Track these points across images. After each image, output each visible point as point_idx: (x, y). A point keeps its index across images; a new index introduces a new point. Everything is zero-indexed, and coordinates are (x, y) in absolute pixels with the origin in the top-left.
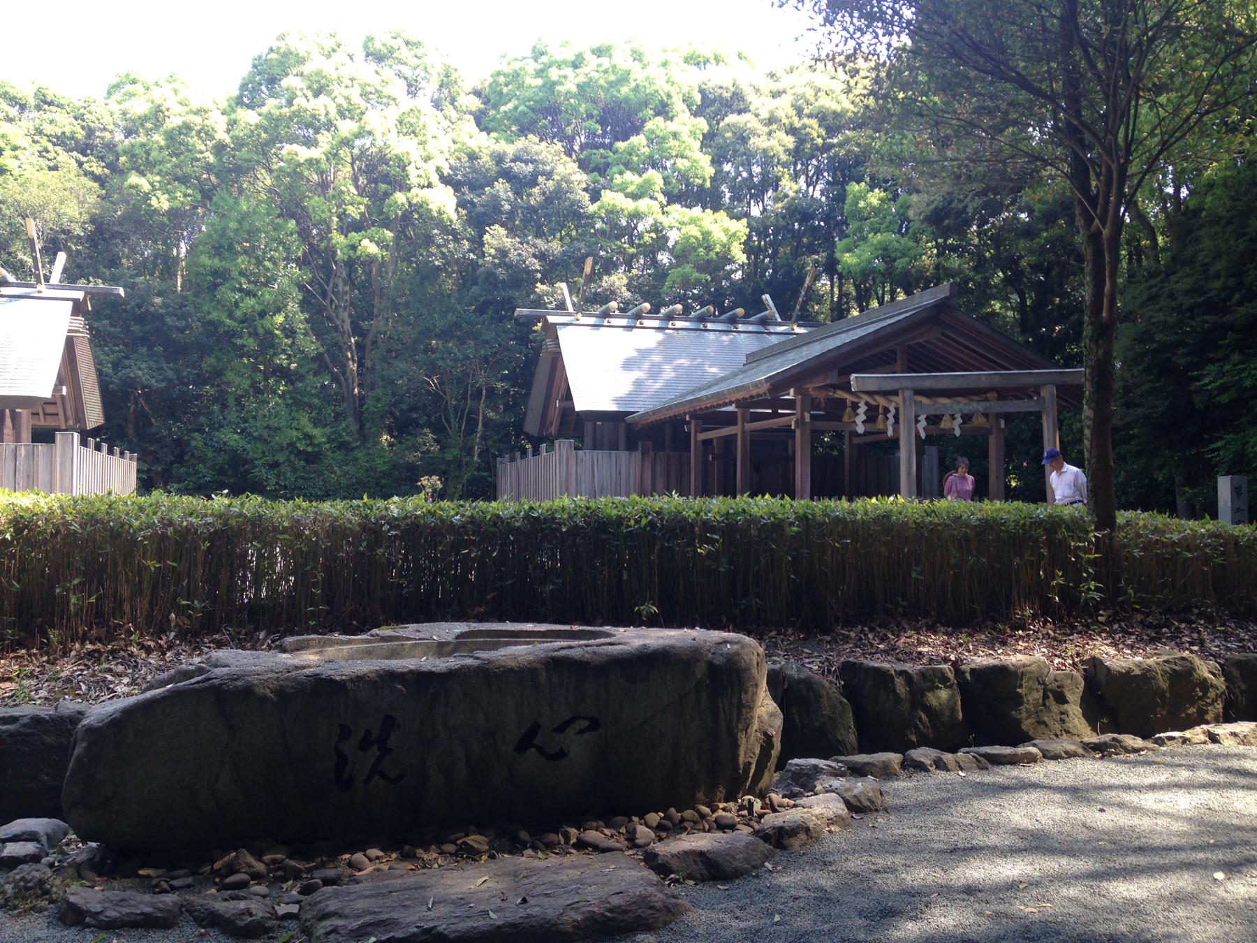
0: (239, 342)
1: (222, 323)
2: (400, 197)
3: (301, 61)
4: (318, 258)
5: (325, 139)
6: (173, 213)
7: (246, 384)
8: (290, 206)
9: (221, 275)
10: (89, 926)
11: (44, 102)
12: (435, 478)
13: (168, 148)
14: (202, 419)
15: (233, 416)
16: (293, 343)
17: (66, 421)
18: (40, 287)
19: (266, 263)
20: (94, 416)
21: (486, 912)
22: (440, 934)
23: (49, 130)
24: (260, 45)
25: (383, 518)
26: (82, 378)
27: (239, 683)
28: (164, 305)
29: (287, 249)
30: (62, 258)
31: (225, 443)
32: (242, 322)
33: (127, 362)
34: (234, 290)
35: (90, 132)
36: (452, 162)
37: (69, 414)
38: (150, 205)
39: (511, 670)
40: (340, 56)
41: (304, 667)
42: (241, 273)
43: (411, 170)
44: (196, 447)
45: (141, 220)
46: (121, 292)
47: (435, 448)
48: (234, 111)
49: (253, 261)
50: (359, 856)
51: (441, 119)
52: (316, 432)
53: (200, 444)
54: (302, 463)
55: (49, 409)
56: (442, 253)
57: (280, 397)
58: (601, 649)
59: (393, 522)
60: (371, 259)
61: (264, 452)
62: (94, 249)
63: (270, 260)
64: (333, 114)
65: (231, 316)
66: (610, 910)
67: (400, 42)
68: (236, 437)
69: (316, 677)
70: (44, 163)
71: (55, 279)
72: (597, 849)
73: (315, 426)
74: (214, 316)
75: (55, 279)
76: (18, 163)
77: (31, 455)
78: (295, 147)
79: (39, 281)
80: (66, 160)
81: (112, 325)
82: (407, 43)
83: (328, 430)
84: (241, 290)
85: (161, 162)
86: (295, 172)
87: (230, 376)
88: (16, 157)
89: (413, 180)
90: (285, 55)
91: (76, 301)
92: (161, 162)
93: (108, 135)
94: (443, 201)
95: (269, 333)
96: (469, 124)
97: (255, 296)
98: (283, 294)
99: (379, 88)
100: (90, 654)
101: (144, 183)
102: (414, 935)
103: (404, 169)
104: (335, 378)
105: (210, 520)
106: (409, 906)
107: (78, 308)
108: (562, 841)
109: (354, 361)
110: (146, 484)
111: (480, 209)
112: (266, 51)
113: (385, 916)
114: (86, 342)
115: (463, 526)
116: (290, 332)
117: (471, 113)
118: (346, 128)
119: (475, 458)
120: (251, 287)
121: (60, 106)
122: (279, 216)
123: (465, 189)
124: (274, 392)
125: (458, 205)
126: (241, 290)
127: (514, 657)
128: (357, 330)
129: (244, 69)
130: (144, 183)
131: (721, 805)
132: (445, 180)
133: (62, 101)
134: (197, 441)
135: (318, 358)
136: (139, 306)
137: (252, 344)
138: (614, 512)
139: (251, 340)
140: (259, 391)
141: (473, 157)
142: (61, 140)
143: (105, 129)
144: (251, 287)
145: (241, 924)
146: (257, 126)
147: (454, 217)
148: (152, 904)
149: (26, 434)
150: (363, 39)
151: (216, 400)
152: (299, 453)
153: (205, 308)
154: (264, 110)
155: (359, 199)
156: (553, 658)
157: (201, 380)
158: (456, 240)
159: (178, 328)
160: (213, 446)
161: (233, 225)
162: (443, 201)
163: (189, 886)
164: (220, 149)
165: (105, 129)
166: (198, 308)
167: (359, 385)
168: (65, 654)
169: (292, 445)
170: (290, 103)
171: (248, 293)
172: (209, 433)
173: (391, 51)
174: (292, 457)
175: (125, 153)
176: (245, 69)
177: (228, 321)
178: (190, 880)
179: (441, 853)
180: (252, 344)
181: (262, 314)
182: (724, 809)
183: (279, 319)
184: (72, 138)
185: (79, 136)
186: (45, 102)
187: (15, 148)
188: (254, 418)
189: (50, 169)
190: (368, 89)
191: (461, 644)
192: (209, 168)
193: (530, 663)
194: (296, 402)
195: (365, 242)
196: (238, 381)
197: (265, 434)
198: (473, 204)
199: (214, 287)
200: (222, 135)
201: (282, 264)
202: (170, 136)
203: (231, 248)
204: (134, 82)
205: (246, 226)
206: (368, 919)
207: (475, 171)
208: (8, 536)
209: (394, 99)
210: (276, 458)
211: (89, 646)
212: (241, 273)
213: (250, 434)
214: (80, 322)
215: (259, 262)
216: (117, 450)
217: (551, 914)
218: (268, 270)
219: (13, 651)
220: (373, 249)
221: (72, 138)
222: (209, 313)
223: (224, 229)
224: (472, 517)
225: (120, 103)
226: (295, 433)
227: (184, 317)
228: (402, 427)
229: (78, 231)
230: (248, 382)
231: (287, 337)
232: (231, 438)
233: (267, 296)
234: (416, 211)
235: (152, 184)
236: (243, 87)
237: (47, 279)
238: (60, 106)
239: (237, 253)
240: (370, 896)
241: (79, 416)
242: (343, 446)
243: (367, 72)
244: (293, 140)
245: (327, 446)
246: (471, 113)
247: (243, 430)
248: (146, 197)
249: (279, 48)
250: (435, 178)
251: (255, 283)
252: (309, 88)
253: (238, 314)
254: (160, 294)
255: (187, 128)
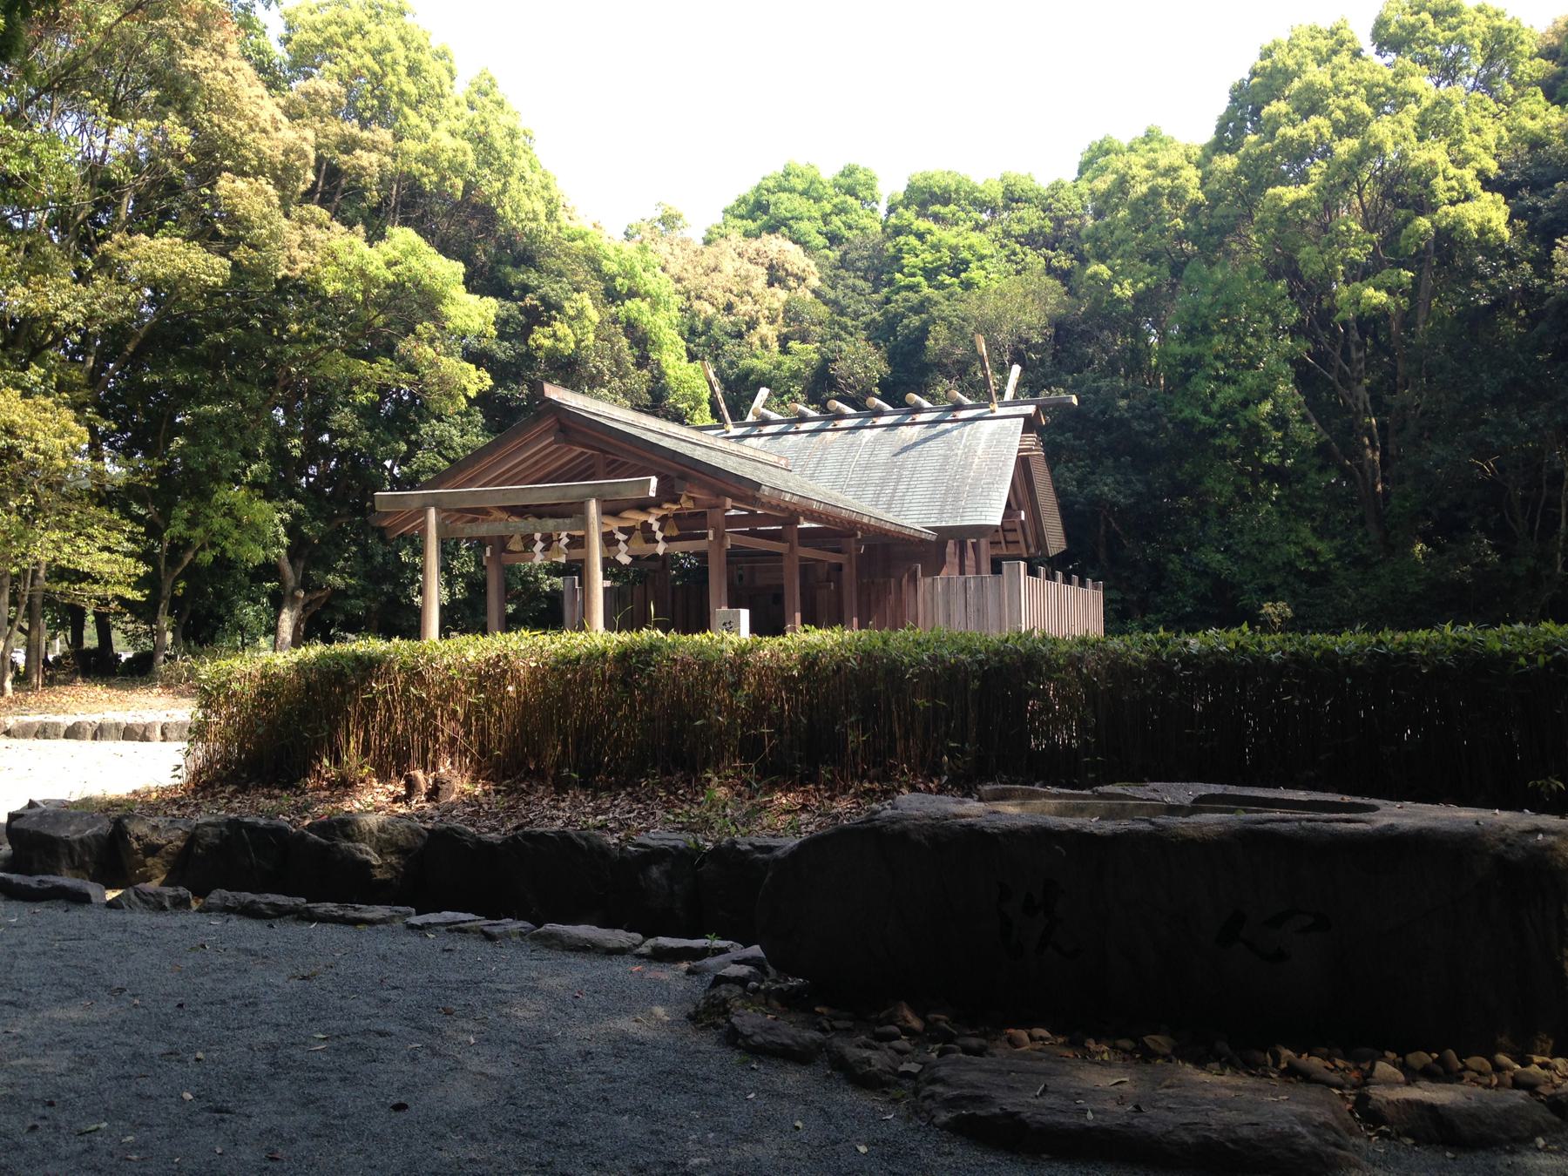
0: (1218, 442)
1: (1196, 421)
2: (1423, 223)
3: (1288, 76)
4: (1318, 320)
5: (1316, 170)
6: (1138, 298)
7: (1228, 490)
8: (1284, 266)
9: (1192, 364)
10: (739, 1047)
11: (1013, 198)
12: (1281, 604)
13: (1133, 221)
14: (1179, 537)
15: (1214, 531)
16: (1286, 434)
17: (1028, 548)
18: (995, 406)
19: (1248, 340)
20: (1056, 542)
21: (1085, 1111)
22: (1022, 1123)
23: (1016, 229)
24: (1240, 67)
25: (1178, 654)
26: (1041, 499)
27: (896, 827)
28: (1130, 408)
29: (1275, 317)
30: (1016, 370)
31: (1206, 565)
32: (1220, 416)
33: (1092, 478)
34: (1208, 378)
35: (1059, 222)
36: (1504, 158)
37: (1030, 540)
38: (1113, 295)
39: (1193, 840)
40: (1343, 58)
41: (963, 816)
42: (1217, 357)
43: (1439, 183)
44: (1173, 571)
45: (1106, 315)
46: (1075, 401)
47: (1494, 558)
48: (1210, 161)
49: (1232, 339)
50: (1023, 1034)
51: (1489, 102)
52: (1321, 547)
53: (1178, 567)
54: (1304, 586)
55: (1011, 537)
56: (1492, 288)
57: (1272, 503)
58: (1325, 826)
59: (1189, 660)
60: (1381, 313)
61: (1254, 574)
62: (1057, 354)
63: (1253, 335)
64: (1327, 132)
65: (1207, 411)
66: (1232, 1141)
67: (1425, 16)
68: (1219, 557)
69: (970, 825)
70: (1012, 267)
71: (1009, 394)
72: (1307, 1078)
73: (1321, 538)
74: (1187, 413)
75: (1009, 394)
76: (983, 273)
77: (981, 586)
78: (1279, 190)
79: (991, 401)
80: (1034, 259)
81: (1075, 438)
82: (1435, 15)
83: (1338, 542)
84: (1217, 378)
85: (1124, 241)
86: (1284, 217)
87: (1209, 483)
88: (983, 268)
89: (1443, 196)
90: (1271, 76)
91: (1027, 417)
92: (1124, 241)
93: (1077, 222)
94: (1489, 213)
95: (1254, 427)
96: (1536, 101)
97: (1235, 382)
98: (1272, 377)
99: (1391, 84)
100: (867, 792)
101: (1103, 270)
102: (995, 1116)
103: (1426, 184)
104: (1345, 473)
105: (981, 656)
106: (1017, 1089)
107: (1030, 424)
108: (1270, 1062)
109: (1374, 449)
110: (1116, 618)
111: (1547, 215)
112: (1247, 77)
113: (982, 1093)
114: (1042, 460)
115: (1284, 665)
116: (1280, 421)
117: (1538, 83)
118: (1345, 148)
119: (1559, 569)
120: (1232, 372)
121: (1028, 201)
122: (1266, 278)
123: (1524, 192)
124: (1266, 498)
125: (1512, 217)
126: (1217, 378)
127: (1199, 826)
128: (1379, 407)
129: (1221, 104)
130: (1103, 270)
131: (1537, 1059)
132: (1488, 184)
133: (1031, 194)
134: (1174, 563)
135: (1322, 449)
136: (1103, 413)
137: (1233, 443)
138: (1498, 646)
139: (1233, 438)
140: (1247, 498)
141: (1536, 143)
142: (1030, 240)
143: (1074, 216)
144: (1232, 372)
145: (860, 1072)
146: (1235, 172)
147: (1506, 233)
148: (793, 1038)
149: (986, 566)
150: (1371, 24)
151: (1195, 514)
152: (1301, 575)
153: (1177, 406)
154: (1242, 151)
155: (1367, 236)
156: (1251, 831)
157: (1178, 489)
158: (1512, 265)
159: (1145, 433)
160: (1192, 570)
161: (1207, 300)
162: (1489, 213)
163: (848, 1029)
164: (1195, 208)
165: (1074, 216)
166: (1168, 406)
167: (1384, 480)
168: (845, 792)
169: (1290, 564)
170: (1273, 134)
171: (1227, 380)
172: (1188, 554)
173: (1413, 29)
174: (1291, 579)
175: (1089, 237)
176: (1222, 104)
177: (1204, 419)
178: (849, 1024)
179: (1114, 1048)
180: (1233, 443)
181: (1245, 404)
182: (1543, 1066)
183: (1267, 407)
184: (1041, 233)
185: (1047, 230)
186: (1013, 200)
187: (982, 258)
188: (1241, 531)
189: (1018, 273)
190: (1376, 90)
191: (1201, 804)
192: (1181, 236)
193: (1220, 834)
194: (1294, 508)
195: (1370, 292)
196: (1219, 487)
197: (1254, 550)
198: (1536, 210)
199: (1187, 378)
200: (1195, 194)
201: (1267, 338)
202: (1135, 208)
203: (1205, 328)
204: (1107, 153)
205: (1222, 297)
206: (966, 1092)
207: (1540, 164)
208: (795, 673)
209: (1414, 95)
210: (1270, 580)
211: (867, 785)
212: (1217, 357)
213: (1236, 553)
214: (1032, 438)
215: (1240, 340)
216: (1075, 578)
217: (1156, 1128)
218: (1250, 347)
219: (802, 784)
220: (1381, 297)
221: (1041, 233)
222: (1181, 411)
223: (1196, 308)
224: (1295, 654)
225: (1090, 181)
226: (1293, 549)
227: (1154, 418)
228: (1447, 529)
229: (1037, 339)
230: (1231, 488)
231: (1277, 429)
232: (1214, 558)
233: (1250, 380)
234: (1448, 240)
235: (1111, 268)
236: (1221, 128)
237: (1001, 393)
238: (1028, 201)
239: (1212, 333)
240: (990, 1071)
241: (1041, 542)
242: (1361, 562)
243: (1379, 66)
244: (1282, 180)
245: (1337, 564)
246: (1538, 83)
247: (1227, 548)
248: (1108, 284)
249: (1263, 68)
250: (1474, 186)
251: (1235, 366)
252: (1296, 110)
253: (1215, 407)
254: (1125, 396)
255: (1154, 192)
